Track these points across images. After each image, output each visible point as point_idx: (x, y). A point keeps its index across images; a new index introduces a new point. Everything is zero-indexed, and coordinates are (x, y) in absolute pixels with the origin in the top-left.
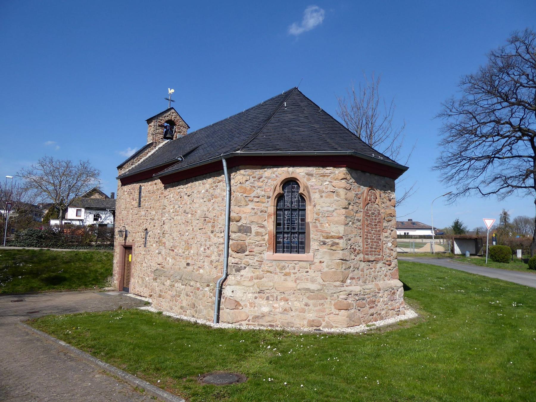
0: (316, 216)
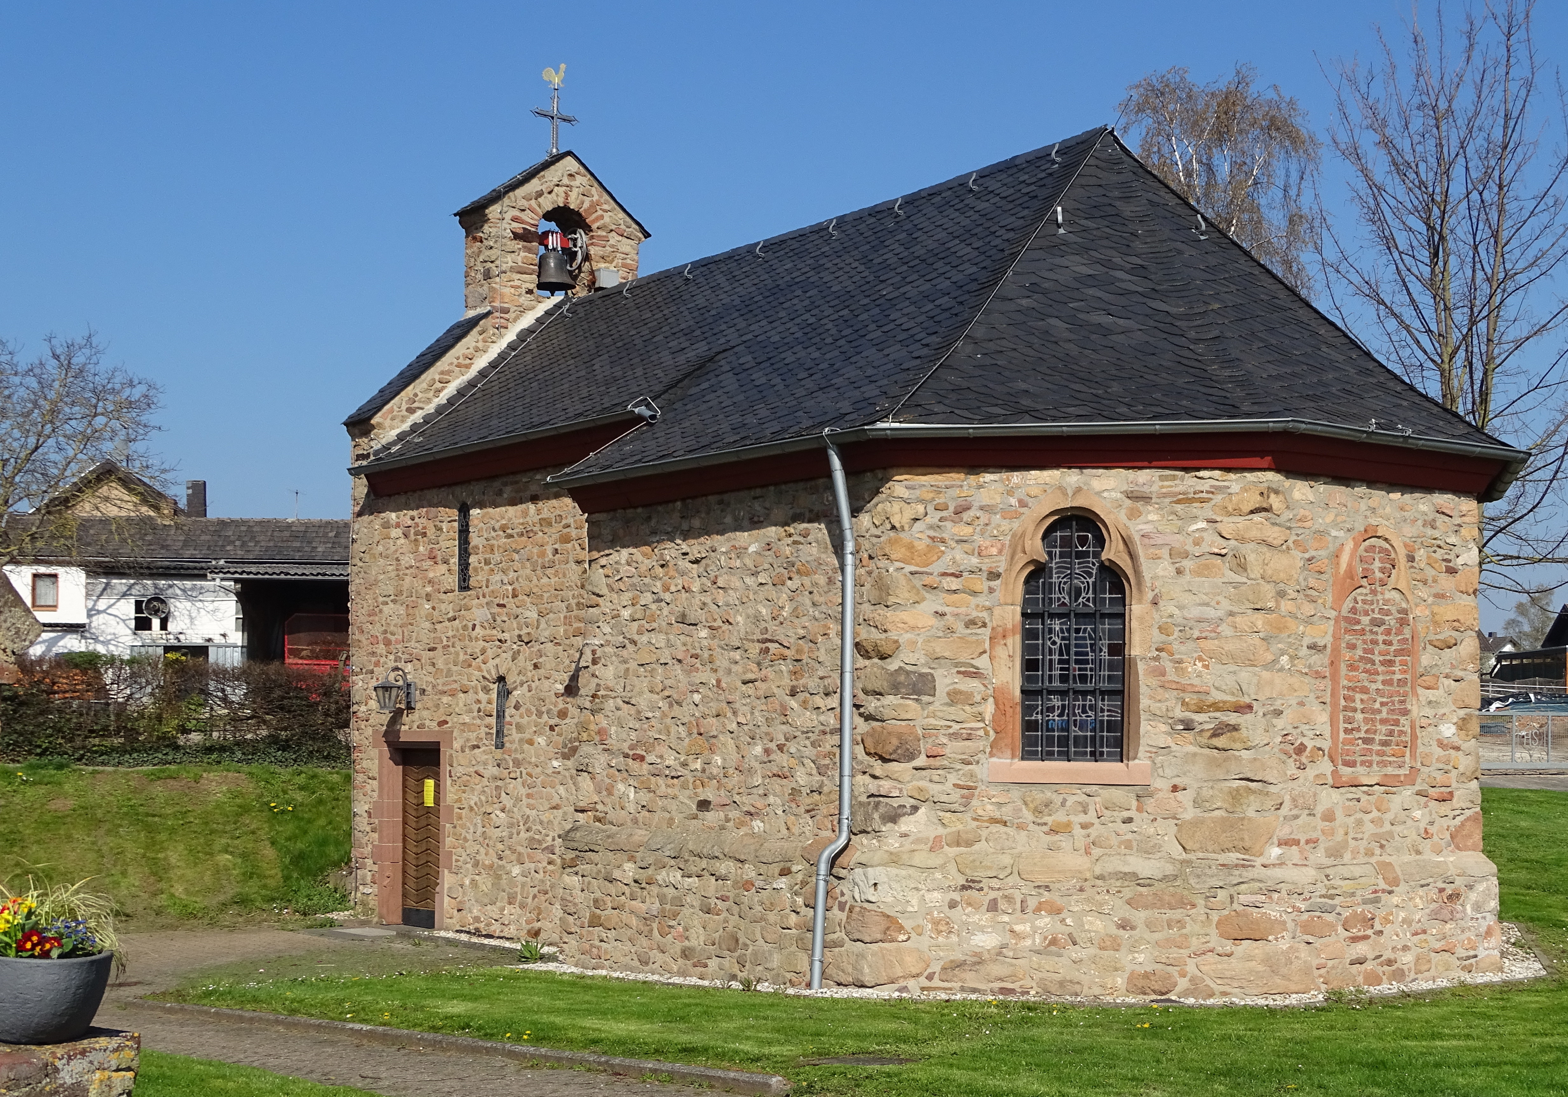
0: (1157, 637)
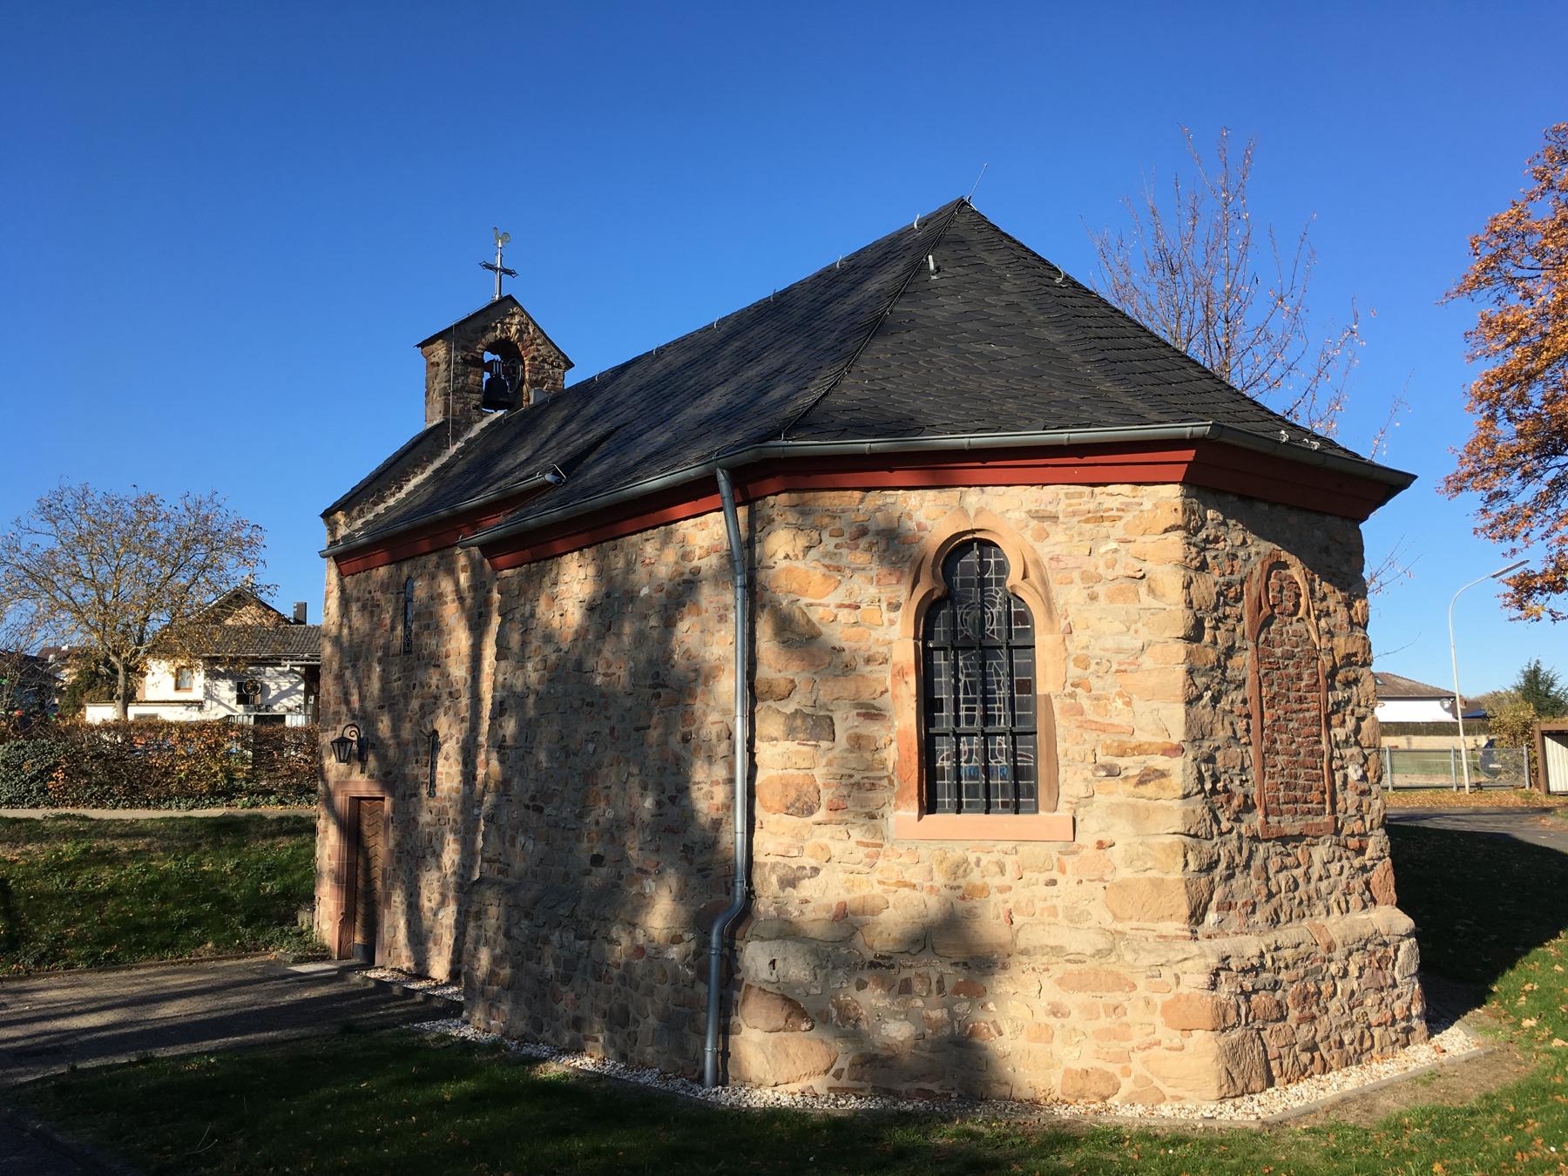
0: (1075, 672)
